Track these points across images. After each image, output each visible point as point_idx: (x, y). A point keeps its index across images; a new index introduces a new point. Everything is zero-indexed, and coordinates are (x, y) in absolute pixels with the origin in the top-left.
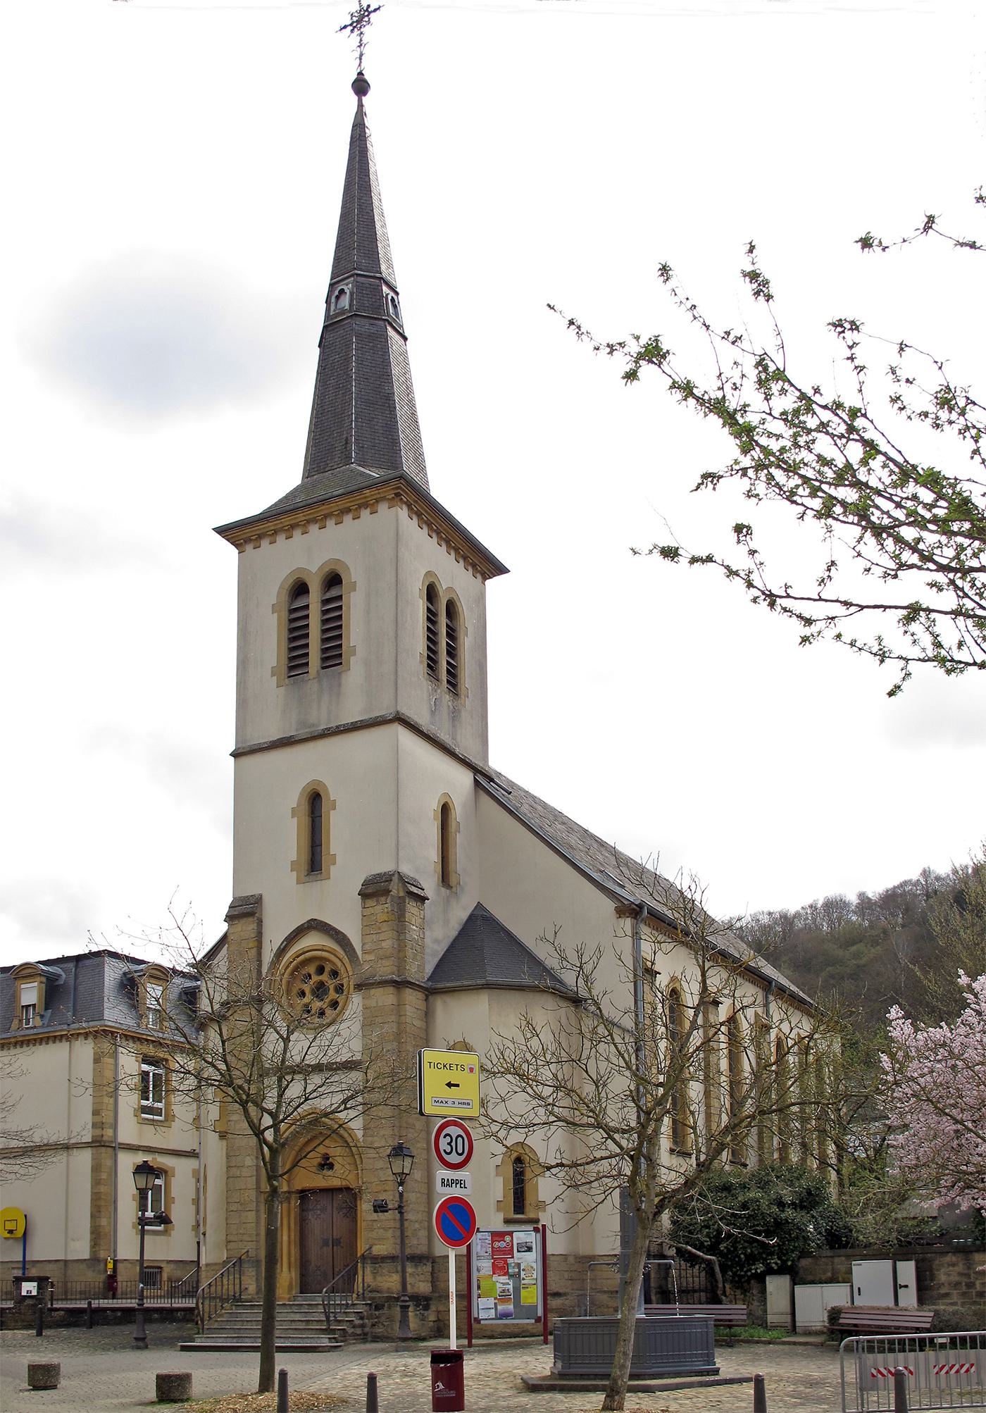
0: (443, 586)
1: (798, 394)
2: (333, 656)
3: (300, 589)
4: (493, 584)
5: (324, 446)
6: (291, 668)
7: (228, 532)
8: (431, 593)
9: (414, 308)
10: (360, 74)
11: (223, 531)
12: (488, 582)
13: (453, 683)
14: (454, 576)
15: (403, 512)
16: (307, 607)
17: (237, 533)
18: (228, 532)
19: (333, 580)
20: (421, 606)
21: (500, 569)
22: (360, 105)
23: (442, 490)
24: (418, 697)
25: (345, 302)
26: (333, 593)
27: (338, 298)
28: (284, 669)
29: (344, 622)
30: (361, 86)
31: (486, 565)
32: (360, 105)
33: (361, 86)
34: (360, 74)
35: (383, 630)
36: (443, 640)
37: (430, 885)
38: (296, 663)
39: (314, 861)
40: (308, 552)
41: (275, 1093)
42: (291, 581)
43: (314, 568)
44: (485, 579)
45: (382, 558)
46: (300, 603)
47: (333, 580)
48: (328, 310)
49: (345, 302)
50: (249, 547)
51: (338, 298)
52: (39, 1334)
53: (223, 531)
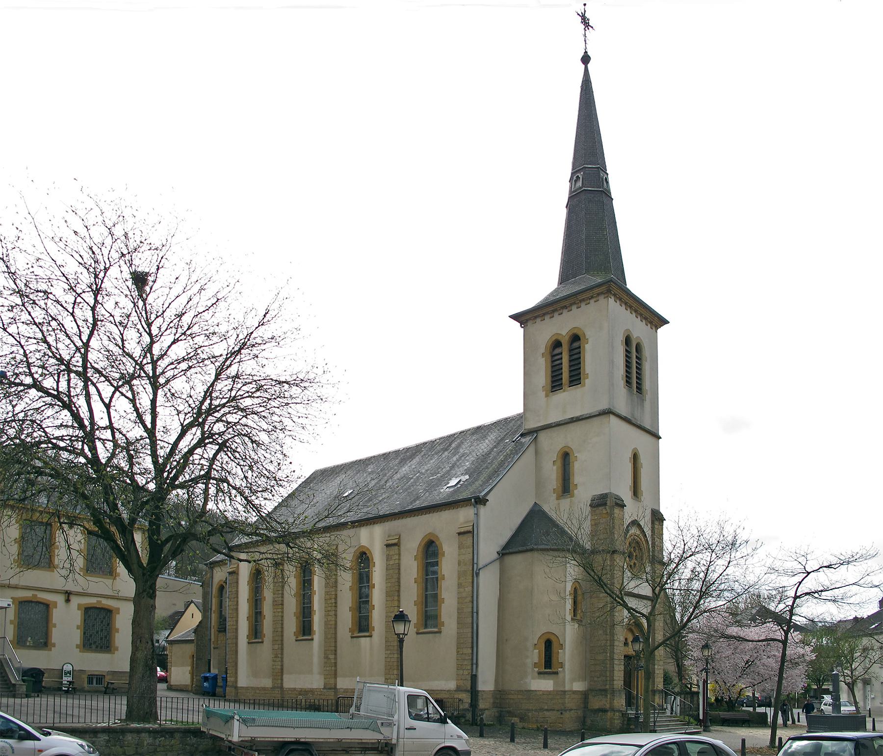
0: (635, 335)
2: (576, 378)
3: (557, 344)
4: (662, 331)
5: (570, 267)
6: (553, 387)
8: (628, 341)
10: (586, 52)
11: (515, 317)
12: (659, 330)
13: (639, 389)
14: (639, 329)
15: (611, 300)
17: (520, 318)
19: (576, 338)
20: (620, 350)
21: (664, 322)
22: (586, 70)
23: (635, 283)
24: (622, 402)
25: (580, 184)
26: (576, 345)
27: (576, 181)
28: (549, 387)
30: (586, 59)
31: (657, 321)
32: (586, 70)
33: (586, 59)
34: (586, 52)
35: (602, 360)
37: (626, 495)
38: (556, 384)
39: (566, 487)
40: (560, 326)
42: (560, 455)
43: (564, 333)
44: (657, 328)
45: (602, 330)
46: (557, 351)
47: (576, 338)
48: (571, 188)
49: (580, 184)
50: (530, 323)
51: (576, 181)
53: (515, 317)
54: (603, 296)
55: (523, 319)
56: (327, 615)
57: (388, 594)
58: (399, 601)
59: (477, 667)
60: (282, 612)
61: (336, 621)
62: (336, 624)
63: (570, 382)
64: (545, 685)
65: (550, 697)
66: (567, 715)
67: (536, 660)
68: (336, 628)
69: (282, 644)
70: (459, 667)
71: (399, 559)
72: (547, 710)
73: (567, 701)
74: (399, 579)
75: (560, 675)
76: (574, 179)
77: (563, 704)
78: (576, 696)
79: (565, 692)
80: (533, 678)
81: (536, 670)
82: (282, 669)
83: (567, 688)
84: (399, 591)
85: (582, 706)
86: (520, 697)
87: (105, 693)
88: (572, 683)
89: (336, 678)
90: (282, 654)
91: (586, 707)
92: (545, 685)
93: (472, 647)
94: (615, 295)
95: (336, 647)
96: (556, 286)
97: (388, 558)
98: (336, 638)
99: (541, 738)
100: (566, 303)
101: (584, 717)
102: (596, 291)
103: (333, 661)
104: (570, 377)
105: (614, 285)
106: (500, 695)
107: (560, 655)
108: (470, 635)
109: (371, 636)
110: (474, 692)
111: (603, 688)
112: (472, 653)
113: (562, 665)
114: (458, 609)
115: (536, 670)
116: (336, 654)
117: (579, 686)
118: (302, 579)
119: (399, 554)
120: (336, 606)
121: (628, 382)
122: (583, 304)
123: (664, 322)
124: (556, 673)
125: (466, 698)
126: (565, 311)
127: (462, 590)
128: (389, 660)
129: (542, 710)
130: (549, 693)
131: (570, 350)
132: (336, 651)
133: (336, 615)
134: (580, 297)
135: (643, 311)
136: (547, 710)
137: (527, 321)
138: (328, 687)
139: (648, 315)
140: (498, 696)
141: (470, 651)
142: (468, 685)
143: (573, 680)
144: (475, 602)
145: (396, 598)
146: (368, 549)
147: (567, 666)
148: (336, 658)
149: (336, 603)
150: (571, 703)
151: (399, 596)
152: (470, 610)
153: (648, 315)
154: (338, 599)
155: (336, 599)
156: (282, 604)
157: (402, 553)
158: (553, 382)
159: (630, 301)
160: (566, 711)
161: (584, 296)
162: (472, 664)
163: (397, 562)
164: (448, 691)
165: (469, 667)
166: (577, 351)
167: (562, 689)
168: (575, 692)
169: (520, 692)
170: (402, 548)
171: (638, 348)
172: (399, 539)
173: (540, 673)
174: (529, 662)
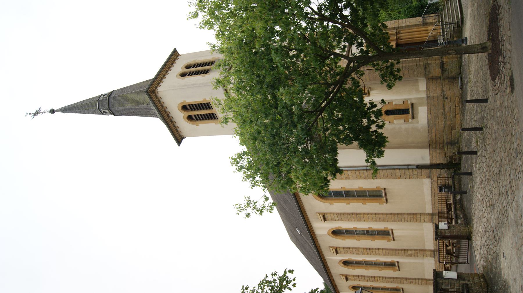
1: (41, 111)
2: (207, 106)
3: (190, 118)
4: (180, 52)
6: (215, 118)
7: (179, 142)
8: (183, 75)
9: (63, 106)
12: (180, 54)
14: (178, 67)
16: (195, 115)
17: (179, 139)
18: (179, 142)
19: (184, 108)
21: (175, 51)
22: (57, 111)
23: (152, 75)
25: (107, 111)
26: (188, 107)
27: (106, 113)
28: (215, 121)
29: (193, 103)
30: (53, 111)
31: (174, 55)
33: (53, 111)
36: (195, 69)
38: (212, 117)
41: (446, 111)
44: (179, 55)
45: (176, 92)
47: (184, 108)
52: (466, 192)
54: (157, 95)
55: (179, 138)
56: (379, 254)
57: (360, 220)
58: (364, 214)
59: (410, 165)
60: (380, 277)
61: (383, 249)
62: (385, 249)
63: (210, 108)
64: (423, 113)
65: (432, 108)
66: (447, 93)
67: (402, 121)
68: (388, 249)
69: (403, 278)
70: (412, 177)
71: (334, 213)
72: (444, 110)
73: (435, 95)
74: (348, 214)
75: (413, 102)
76: (104, 113)
77: (438, 97)
78: (431, 87)
79: (428, 97)
80: (418, 122)
81: (410, 120)
82: (421, 279)
83: (425, 96)
84: (356, 214)
85: (439, 81)
86: (433, 130)
87: (458, 257)
88: (420, 91)
89: (425, 250)
90: (410, 279)
91: (440, 78)
92: (423, 113)
93: (395, 169)
94: (156, 87)
95: (402, 250)
96: (158, 118)
97: (333, 220)
98: (395, 250)
99: (464, 177)
100: (165, 115)
101: (449, 78)
102: (155, 99)
103: (413, 252)
104: (207, 109)
105: (151, 88)
106: (432, 145)
107: (398, 103)
108: (385, 171)
109: (392, 230)
110: (432, 166)
111: (423, 68)
112: (400, 169)
113: (405, 101)
114: (365, 179)
115: (410, 120)
116: (408, 250)
117: (422, 85)
118: (355, 265)
119: (330, 213)
120: (372, 249)
121: (206, 72)
122: (165, 105)
123: (175, 51)
124: (412, 105)
125: (435, 172)
126: (170, 115)
127: (350, 177)
128: (409, 220)
129: (444, 114)
130: (429, 110)
131: (192, 110)
132: (405, 250)
133: (378, 249)
134: (160, 108)
135: (167, 67)
136: (444, 110)
137: (180, 136)
138: (433, 255)
139: (170, 63)
140: (434, 146)
141: (398, 171)
142: (425, 171)
143: (418, 91)
144: (359, 168)
145: (362, 216)
146: (330, 230)
147: (405, 97)
148: (411, 250)
149: (370, 249)
150: (437, 92)
151: (360, 214)
152: (365, 172)
153: (170, 63)
154: (367, 247)
155: (367, 249)
156: (374, 277)
157: (329, 212)
158: (212, 119)
159: (161, 76)
160: (444, 95)
161: (159, 105)
162: (409, 169)
163: (335, 215)
164: (432, 183)
165: (411, 171)
166: (191, 106)
167: (426, 99)
168: (428, 88)
169: (430, 131)
170: (325, 211)
171: (188, 67)
172: (319, 213)
173: (413, 117)
174: (404, 126)
